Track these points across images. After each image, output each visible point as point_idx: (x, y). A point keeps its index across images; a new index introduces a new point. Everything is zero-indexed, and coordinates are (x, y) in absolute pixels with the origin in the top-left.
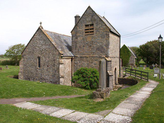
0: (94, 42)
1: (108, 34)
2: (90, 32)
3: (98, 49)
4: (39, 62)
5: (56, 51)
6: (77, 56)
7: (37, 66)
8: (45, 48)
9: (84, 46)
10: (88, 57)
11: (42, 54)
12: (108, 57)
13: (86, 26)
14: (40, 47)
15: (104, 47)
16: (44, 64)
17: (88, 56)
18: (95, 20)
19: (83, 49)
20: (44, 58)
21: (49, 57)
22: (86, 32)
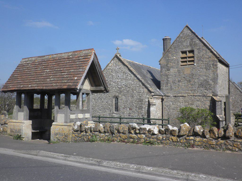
0: (195, 75)
1: (215, 64)
2: (189, 61)
3: (201, 85)
4: (117, 104)
5: (143, 88)
6: (169, 95)
7: (113, 110)
8: (125, 84)
9: (179, 81)
10: (185, 96)
11: (121, 92)
12: (216, 96)
13: (183, 52)
14: (118, 82)
15: (211, 82)
16: (125, 106)
17: (186, 95)
18: (195, 44)
19: (179, 85)
20: (124, 97)
21: (133, 97)
22: (182, 62)
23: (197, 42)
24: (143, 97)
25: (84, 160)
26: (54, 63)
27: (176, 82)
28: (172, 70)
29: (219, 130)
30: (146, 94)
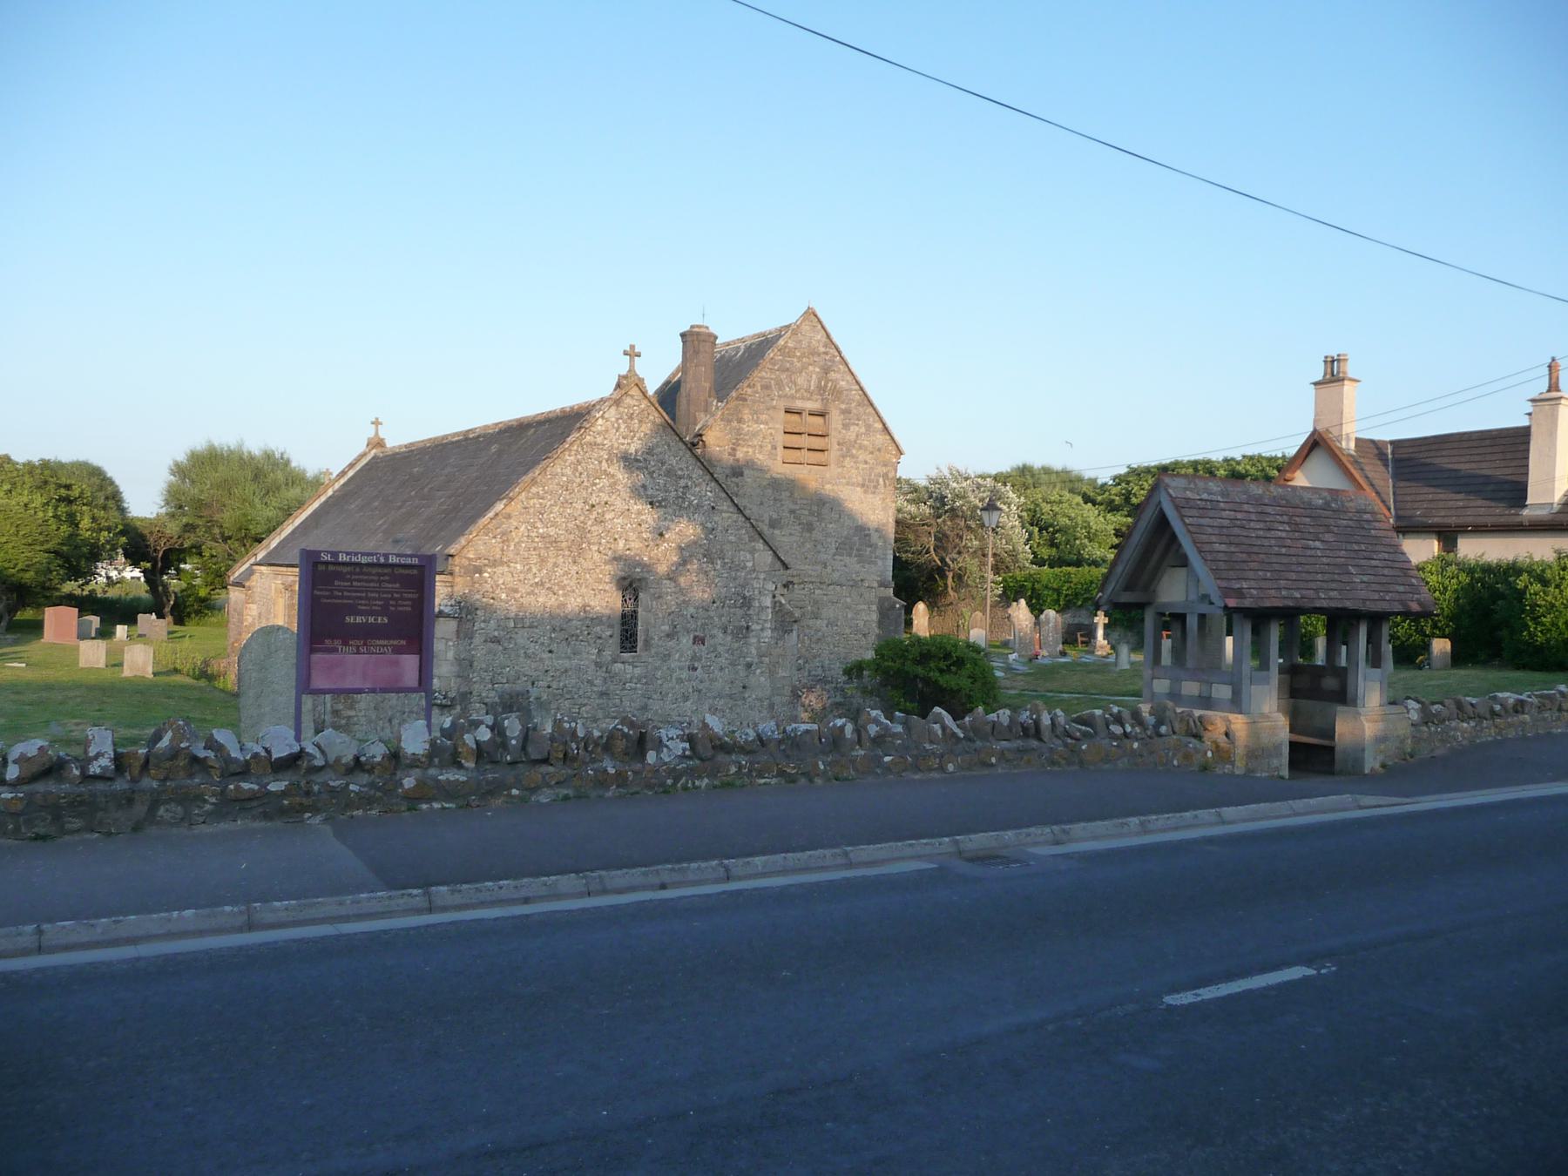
5: (753, 551)
18: (837, 393)
23: (843, 383)
24: (754, 589)
26: (1308, 519)
29: (476, 740)
30: (762, 576)
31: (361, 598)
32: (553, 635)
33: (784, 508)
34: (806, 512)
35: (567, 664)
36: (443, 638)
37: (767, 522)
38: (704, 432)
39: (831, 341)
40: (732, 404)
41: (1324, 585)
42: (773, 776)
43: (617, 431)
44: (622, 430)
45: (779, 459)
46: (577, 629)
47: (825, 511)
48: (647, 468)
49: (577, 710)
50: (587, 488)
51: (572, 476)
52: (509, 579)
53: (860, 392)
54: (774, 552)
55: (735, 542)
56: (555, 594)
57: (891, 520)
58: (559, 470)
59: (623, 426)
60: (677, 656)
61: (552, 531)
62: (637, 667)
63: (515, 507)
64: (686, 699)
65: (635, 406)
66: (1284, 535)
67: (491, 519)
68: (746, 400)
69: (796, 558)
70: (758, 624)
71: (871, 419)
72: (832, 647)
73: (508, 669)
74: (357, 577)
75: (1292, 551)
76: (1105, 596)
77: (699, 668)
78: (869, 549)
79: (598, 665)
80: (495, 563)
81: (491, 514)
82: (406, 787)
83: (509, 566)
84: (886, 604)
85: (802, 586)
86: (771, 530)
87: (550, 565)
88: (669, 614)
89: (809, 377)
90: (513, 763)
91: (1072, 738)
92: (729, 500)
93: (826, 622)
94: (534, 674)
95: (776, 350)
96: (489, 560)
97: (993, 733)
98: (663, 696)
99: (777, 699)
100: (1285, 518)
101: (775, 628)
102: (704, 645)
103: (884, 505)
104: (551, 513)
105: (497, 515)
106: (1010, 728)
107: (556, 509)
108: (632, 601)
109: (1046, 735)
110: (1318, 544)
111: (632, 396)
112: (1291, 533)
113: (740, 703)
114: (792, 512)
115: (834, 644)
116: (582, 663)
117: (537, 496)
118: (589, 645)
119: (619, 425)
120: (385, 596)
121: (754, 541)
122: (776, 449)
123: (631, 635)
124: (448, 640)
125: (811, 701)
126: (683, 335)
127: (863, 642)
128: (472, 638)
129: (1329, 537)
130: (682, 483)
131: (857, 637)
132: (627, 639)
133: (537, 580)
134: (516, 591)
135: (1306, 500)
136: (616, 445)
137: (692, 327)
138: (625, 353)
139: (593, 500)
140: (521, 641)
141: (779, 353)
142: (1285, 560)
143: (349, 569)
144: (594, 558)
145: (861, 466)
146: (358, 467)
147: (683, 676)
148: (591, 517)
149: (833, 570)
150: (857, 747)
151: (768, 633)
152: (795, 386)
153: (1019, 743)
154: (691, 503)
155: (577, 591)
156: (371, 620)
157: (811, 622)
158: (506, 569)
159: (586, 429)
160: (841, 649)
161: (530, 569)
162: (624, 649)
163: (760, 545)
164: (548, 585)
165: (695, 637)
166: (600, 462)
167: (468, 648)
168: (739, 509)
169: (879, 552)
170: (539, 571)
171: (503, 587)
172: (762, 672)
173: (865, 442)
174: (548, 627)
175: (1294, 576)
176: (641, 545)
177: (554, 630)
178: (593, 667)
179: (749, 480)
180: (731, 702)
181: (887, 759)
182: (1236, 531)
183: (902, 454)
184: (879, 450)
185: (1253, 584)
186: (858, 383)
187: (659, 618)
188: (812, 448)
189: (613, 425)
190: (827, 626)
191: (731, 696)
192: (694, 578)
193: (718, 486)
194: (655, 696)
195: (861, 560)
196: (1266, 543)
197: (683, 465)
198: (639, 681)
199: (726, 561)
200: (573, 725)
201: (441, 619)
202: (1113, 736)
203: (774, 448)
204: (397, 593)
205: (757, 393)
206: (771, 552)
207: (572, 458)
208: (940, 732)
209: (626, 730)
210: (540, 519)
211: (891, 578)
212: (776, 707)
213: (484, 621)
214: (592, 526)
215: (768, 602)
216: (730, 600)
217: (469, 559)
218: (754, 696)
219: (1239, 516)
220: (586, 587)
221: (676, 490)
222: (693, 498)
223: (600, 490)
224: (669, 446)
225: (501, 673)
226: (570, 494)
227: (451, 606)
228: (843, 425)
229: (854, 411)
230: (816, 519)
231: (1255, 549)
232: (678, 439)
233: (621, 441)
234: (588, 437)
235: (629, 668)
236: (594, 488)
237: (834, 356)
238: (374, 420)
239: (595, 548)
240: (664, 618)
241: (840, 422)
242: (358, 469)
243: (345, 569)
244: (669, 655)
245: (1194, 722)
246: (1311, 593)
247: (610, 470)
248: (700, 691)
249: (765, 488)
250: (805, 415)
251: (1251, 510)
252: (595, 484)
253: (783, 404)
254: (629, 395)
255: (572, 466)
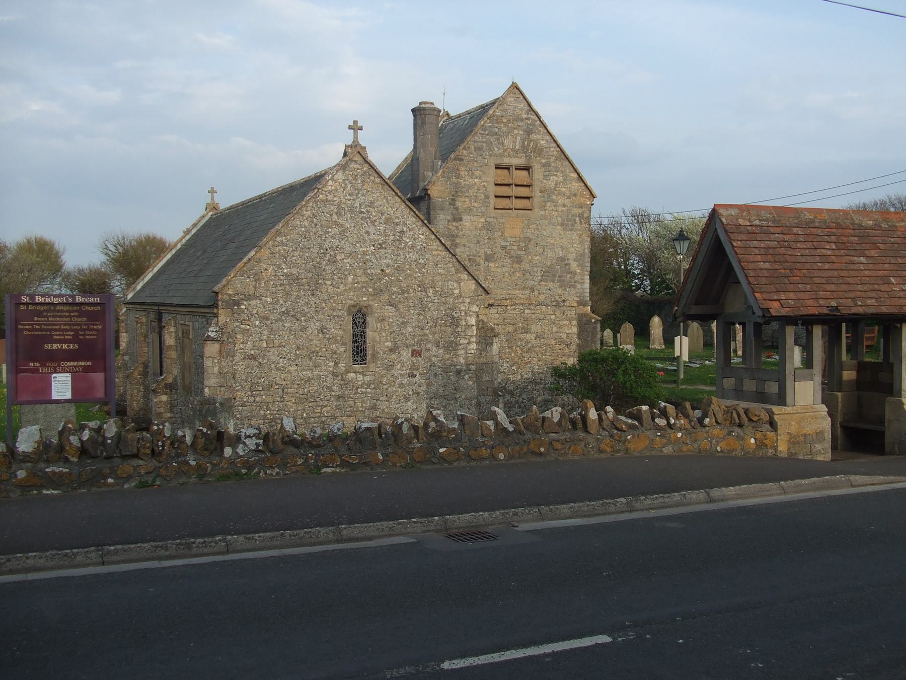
5: (459, 281)
14: (364, 253)
18: (539, 151)
23: (542, 142)
24: (461, 311)
25: (584, 506)
26: (856, 238)
27: (478, 259)
28: (467, 221)
30: (468, 300)
31: (56, 330)
32: (298, 352)
33: (497, 245)
34: (516, 248)
35: (310, 374)
36: (210, 357)
37: (483, 256)
38: (428, 188)
39: (532, 108)
40: (450, 164)
41: (864, 294)
42: (337, 466)
43: (344, 190)
44: (348, 189)
45: (492, 206)
46: (317, 347)
47: (531, 246)
48: (369, 218)
49: (319, 410)
50: (321, 236)
51: (309, 227)
52: (261, 309)
53: (558, 149)
54: (477, 281)
55: (444, 274)
56: (298, 320)
57: (587, 251)
58: (298, 223)
59: (349, 186)
60: (399, 366)
61: (294, 271)
62: (366, 375)
63: (265, 253)
64: (407, 399)
65: (358, 169)
66: (829, 252)
67: (245, 263)
68: (462, 160)
69: (508, 285)
70: (465, 338)
71: (568, 170)
72: (540, 355)
73: (263, 380)
74: (52, 314)
75: (835, 266)
76: (680, 310)
77: (418, 375)
78: (569, 276)
79: (335, 375)
80: (249, 298)
81: (245, 260)
82: (19, 478)
83: (261, 300)
84: (584, 319)
85: (514, 307)
86: (487, 263)
87: (293, 298)
88: (391, 333)
89: (513, 141)
90: (108, 458)
91: (618, 429)
92: (438, 241)
93: (534, 335)
94: (284, 383)
95: (486, 119)
96: (245, 295)
97: (542, 426)
98: (389, 398)
99: (482, 399)
100: (833, 238)
101: (479, 342)
102: (421, 357)
103: (580, 239)
104: (293, 256)
105: (250, 260)
106: (559, 423)
107: (297, 254)
108: (361, 323)
109: (593, 428)
110: (862, 259)
111: (356, 162)
112: (837, 251)
113: (452, 402)
114: (504, 248)
115: (542, 353)
116: (322, 373)
117: (283, 244)
118: (327, 359)
119: (346, 185)
120: (75, 327)
121: (459, 273)
122: (488, 198)
123: (361, 350)
124: (214, 358)
125: (523, 399)
126: (413, 110)
127: (566, 351)
128: (233, 357)
129: (873, 253)
130: (399, 228)
131: (561, 347)
132: (358, 354)
133: (283, 309)
134: (267, 319)
135: (857, 222)
136: (344, 200)
137: (421, 103)
138: (350, 128)
139: (327, 245)
140: (272, 357)
141: (488, 121)
142: (826, 274)
143: (45, 308)
144: (329, 291)
145: (560, 209)
146: (199, 226)
147: (404, 382)
148: (325, 258)
149: (540, 294)
150: (415, 441)
151: (474, 346)
152: (503, 147)
153: (568, 435)
154: (406, 244)
155: (316, 317)
156: (65, 346)
157: (522, 336)
158: (258, 302)
159: (319, 189)
160: (548, 357)
161: (277, 302)
162: (356, 361)
163: (465, 276)
164: (292, 313)
165: (413, 351)
166: (331, 215)
167: (230, 364)
168: (446, 248)
169: (577, 278)
170: (285, 302)
171: (257, 316)
172: (469, 377)
173: (564, 189)
174: (294, 346)
175: (833, 287)
176: (367, 279)
177: (298, 348)
178: (331, 377)
179: (467, 224)
180: (445, 402)
181: (441, 450)
182: (782, 251)
183: (594, 198)
184: (575, 195)
185: (792, 295)
186: (555, 141)
187: (383, 337)
188: (519, 196)
189: (341, 186)
190: (535, 339)
191: (444, 397)
192: (411, 304)
193: (427, 230)
194: (381, 398)
195: (563, 285)
196: (811, 259)
197: (399, 214)
198: (369, 387)
199: (437, 289)
200: (161, 427)
201: (208, 342)
202: (658, 428)
203: (487, 197)
204: (85, 325)
205: (472, 154)
206: (474, 281)
207: (309, 212)
208: (492, 428)
209: (205, 430)
210: (284, 262)
211: (588, 299)
212: (482, 405)
213: (243, 343)
214: (326, 265)
215: (473, 321)
216: (441, 321)
217: (230, 295)
218: (463, 397)
219: (787, 237)
220: (323, 314)
221: (394, 235)
222: (408, 240)
223: (332, 237)
224: (387, 199)
225: (258, 383)
226: (308, 241)
227: (216, 331)
228: (544, 176)
229: (553, 164)
230: (524, 253)
231: (799, 266)
232: (394, 194)
233: (349, 197)
234: (321, 196)
235: (360, 377)
236: (327, 236)
237: (535, 121)
238: (210, 189)
239: (329, 283)
240: (387, 336)
241: (541, 174)
242: (199, 227)
243: (42, 308)
244: (392, 366)
245: (739, 415)
246: (849, 302)
247: (339, 221)
248: (418, 393)
249: (480, 229)
250: (513, 169)
251: (800, 233)
252: (328, 232)
253: (492, 162)
254: (354, 161)
255: (309, 219)
